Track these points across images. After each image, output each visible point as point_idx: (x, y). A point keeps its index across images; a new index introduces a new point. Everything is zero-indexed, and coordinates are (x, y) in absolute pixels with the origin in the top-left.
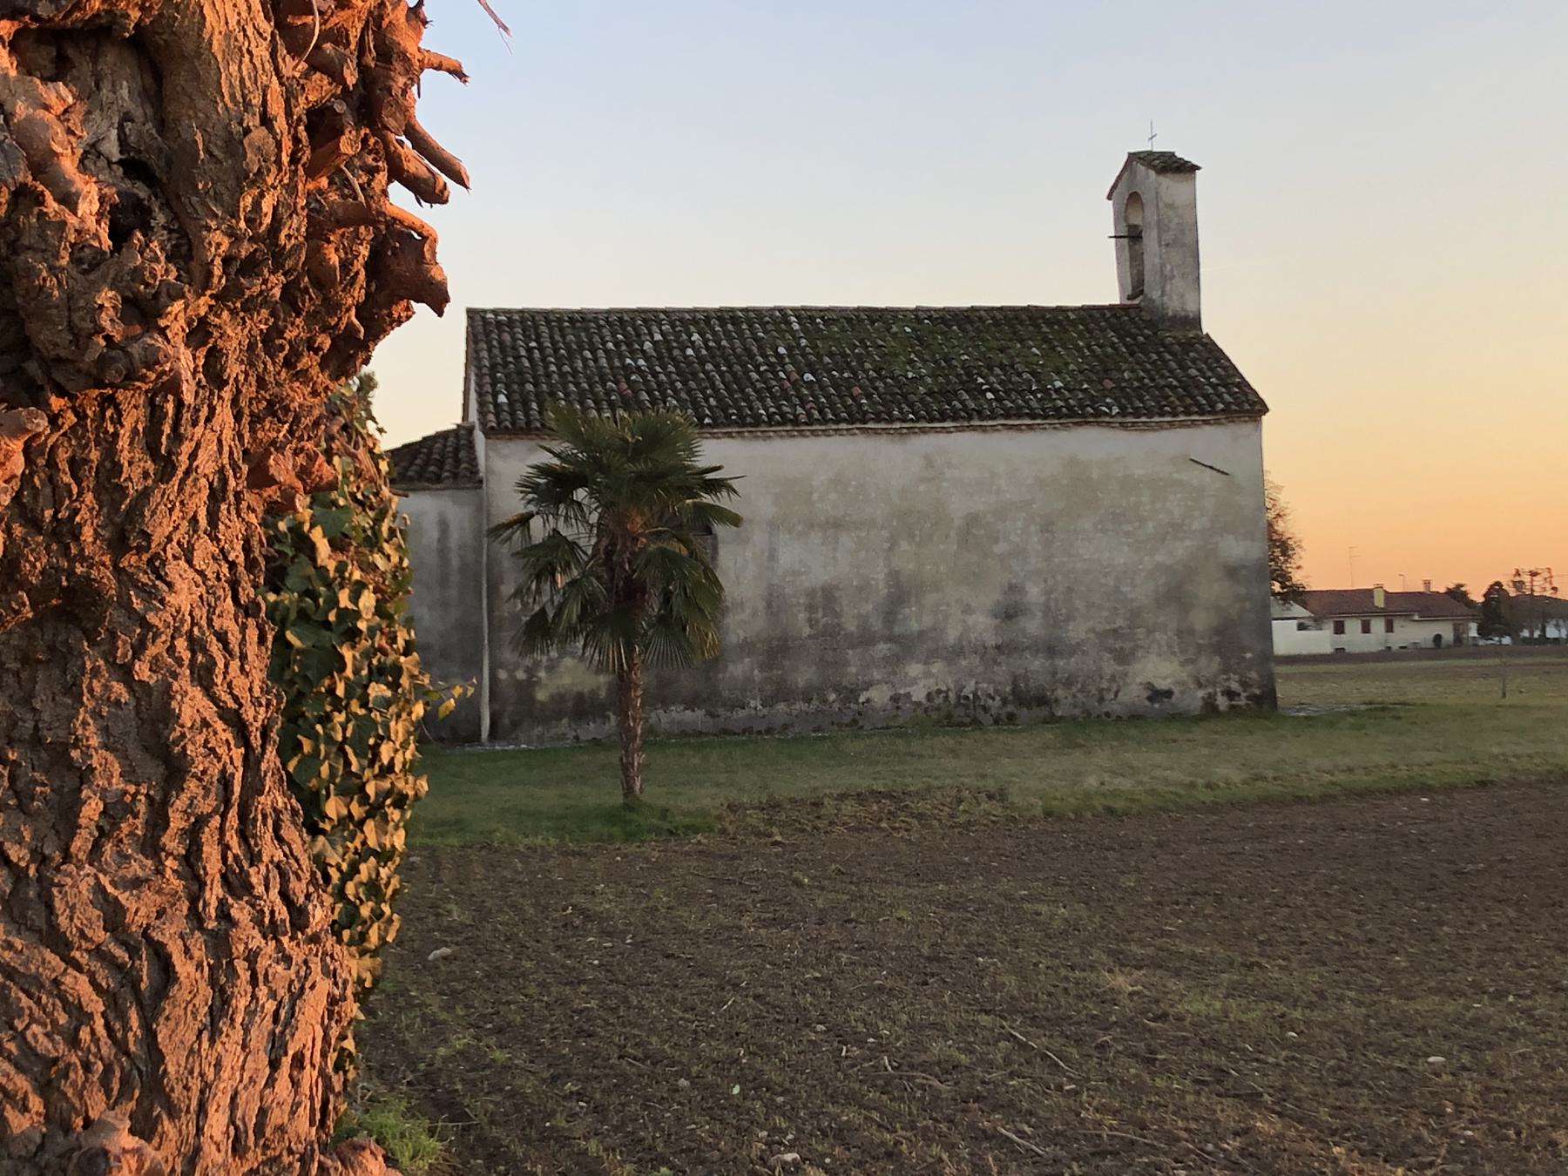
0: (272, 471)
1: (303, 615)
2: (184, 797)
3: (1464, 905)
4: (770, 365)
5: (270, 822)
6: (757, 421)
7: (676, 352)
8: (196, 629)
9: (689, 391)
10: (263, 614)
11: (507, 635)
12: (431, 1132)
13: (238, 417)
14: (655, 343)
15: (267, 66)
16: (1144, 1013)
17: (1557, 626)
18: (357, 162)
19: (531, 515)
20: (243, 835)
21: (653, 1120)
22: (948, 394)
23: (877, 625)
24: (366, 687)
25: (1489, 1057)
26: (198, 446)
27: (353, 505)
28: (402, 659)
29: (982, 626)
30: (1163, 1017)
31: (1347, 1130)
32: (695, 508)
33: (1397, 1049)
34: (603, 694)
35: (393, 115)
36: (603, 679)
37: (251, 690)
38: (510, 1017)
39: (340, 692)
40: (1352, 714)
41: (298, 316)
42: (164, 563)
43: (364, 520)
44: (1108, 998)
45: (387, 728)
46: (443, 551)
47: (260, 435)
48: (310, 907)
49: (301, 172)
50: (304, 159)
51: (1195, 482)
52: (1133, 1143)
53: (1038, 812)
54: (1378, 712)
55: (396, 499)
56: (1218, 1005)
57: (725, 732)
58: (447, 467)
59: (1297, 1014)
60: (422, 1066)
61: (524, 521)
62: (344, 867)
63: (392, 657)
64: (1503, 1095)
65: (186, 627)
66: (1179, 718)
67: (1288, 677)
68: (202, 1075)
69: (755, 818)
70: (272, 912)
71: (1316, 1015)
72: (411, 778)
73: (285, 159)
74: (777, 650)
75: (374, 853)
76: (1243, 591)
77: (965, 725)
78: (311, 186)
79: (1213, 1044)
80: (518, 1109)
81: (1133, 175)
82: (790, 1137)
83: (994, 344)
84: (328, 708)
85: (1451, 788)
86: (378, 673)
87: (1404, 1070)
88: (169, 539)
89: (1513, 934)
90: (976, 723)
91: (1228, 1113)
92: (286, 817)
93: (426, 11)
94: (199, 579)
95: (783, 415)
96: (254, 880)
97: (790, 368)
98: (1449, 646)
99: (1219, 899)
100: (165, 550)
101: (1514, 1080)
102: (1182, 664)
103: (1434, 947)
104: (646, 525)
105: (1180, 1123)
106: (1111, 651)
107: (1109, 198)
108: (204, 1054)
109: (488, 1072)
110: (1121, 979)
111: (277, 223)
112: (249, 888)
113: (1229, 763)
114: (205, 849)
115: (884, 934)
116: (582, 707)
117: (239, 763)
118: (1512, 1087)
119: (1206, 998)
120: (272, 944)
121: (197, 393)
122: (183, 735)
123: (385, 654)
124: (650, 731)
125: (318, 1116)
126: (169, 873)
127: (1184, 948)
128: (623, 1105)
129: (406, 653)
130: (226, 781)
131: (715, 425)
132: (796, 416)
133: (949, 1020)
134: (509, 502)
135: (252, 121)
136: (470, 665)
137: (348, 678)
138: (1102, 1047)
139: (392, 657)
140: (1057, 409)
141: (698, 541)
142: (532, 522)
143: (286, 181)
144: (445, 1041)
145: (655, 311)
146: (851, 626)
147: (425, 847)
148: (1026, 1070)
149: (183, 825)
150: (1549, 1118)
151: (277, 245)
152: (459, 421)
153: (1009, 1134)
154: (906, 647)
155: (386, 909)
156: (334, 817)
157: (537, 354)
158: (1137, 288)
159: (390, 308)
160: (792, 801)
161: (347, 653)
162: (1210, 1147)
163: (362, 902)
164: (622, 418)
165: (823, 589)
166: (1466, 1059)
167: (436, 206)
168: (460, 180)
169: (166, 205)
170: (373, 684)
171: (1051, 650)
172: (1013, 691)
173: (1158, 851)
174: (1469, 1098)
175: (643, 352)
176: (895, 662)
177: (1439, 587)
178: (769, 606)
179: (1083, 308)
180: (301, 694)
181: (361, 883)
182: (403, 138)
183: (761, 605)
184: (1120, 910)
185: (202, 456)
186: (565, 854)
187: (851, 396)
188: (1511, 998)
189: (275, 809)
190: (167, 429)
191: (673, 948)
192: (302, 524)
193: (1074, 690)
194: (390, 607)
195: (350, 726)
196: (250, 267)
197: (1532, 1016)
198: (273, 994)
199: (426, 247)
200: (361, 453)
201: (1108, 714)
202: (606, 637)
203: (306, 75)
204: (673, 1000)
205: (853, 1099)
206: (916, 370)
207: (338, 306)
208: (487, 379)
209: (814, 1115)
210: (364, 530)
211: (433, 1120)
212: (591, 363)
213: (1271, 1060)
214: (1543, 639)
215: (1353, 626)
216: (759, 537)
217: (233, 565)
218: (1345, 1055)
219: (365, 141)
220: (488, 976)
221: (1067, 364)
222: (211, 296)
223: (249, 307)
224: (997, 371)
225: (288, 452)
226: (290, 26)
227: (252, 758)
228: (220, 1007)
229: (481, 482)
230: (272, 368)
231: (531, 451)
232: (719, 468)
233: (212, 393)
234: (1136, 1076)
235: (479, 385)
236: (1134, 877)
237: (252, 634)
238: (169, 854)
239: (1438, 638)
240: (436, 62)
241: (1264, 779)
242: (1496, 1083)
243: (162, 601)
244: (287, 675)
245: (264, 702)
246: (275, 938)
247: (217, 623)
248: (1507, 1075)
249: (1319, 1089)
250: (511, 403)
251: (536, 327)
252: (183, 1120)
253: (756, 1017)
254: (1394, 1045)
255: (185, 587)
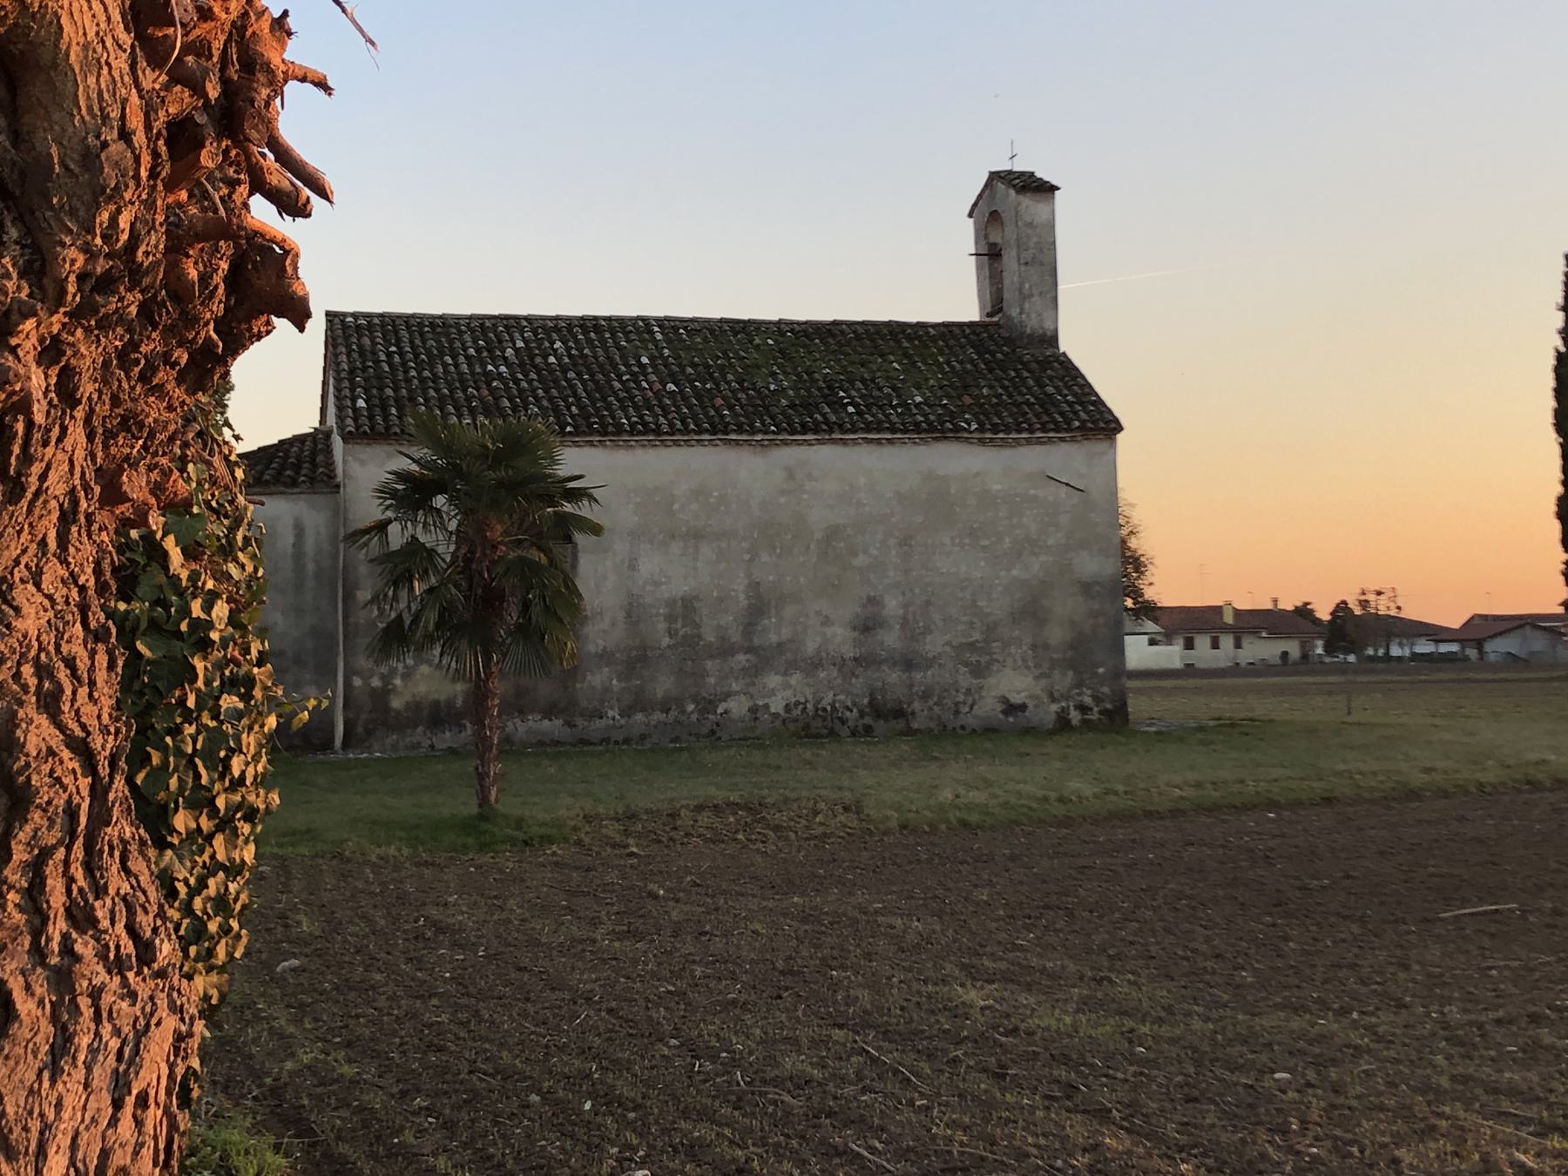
0: (124, 487)
1: (154, 625)
2: (28, 828)
3: (1309, 921)
4: (633, 374)
5: (117, 853)
6: (619, 430)
7: (538, 360)
8: (43, 656)
9: (551, 399)
10: (113, 640)
11: (363, 642)
12: (277, 1148)
13: (90, 437)
14: (517, 350)
15: (126, 78)
16: (995, 1027)
17: (1401, 645)
18: (218, 175)
19: (389, 521)
20: (89, 868)
21: (503, 1136)
22: (809, 406)
23: (736, 636)
24: (218, 698)
25: (1333, 1074)
26: (48, 467)
27: (207, 513)
28: (256, 670)
29: (841, 639)
30: (1014, 1031)
31: (1195, 1146)
32: (555, 517)
33: (1243, 1066)
34: (459, 702)
35: (255, 127)
36: (460, 687)
37: (99, 717)
38: (359, 1030)
39: (191, 703)
40: (1201, 729)
41: (154, 330)
42: (11, 587)
43: (218, 529)
44: (959, 1012)
45: (238, 740)
46: (299, 567)
47: (113, 450)
48: (157, 941)
49: (160, 187)
50: (164, 174)
51: (1051, 498)
52: (983, 1159)
53: (893, 824)
54: (1229, 729)
55: (251, 507)
56: (1068, 1020)
57: (583, 742)
58: (304, 472)
59: (1145, 1029)
60: (268, 1080)
61: (382, 527)
62: (192, 881)
63: (245, 668)
64: (1346, 1112)
65: (33, 653)
66: (1029, 731)
67: (1139, 691)
68: (42, 1115)
69: (612, 830)
70: (118, 947)
71: (1164, 1031)
72: (262, 792)
73: (144, 174)
74: (637, 660)
75: (223, 867)
76: (1097, 606)
77: (822, 736)
78: (170, 200)
79: (1065, 1060)
80: (366, 1125)
81: (992, 197)
82: (641, 1153)
83: (856, 358)
84: (179, 720)
85: (1297, 804)
86: (230, 685)
87: (1252, 1087)
88: (17, 562)
89: (1356, 950)
90: (832, 733)
91: (1077, 1129)
92: (133, 847)
93: (291, 22)
94: (46, 603)
95: (645, 424)
96: (99, 914)
97: (653, 378)
98: (1295, 664)
99: (1070, 913)
100: (12, 574)
101: (1358, 1097)
102: (1037, 678)
103: (1279, 963)
104: (506, 533)
105: (1030, 1140)
106: (967, 665)
107: (970, 215)
108: (44, 1094)
109: (335, 1087)
110: (973, 994)
111: (134, 240)
112: (94, 922)
113: (1083, 778)
114: (49, 881)
115: (738, 947)
116: (438, 716)
117: (85, 792)
118: (1355, 1103)
119: (1057, 1011)
120: (117, 980)
121: (48, 413)
122: (28, 765)
123: (238, 665)
124: (507, 739)
125: (162, 1157)
126: (10, 907)
127: (1034, 962)
128: (472, 1121)
129: (259, 665)
130: (72, 813)
131: (576, 433)
132: (659, 426)
133: (804, 1034)
134: (367, 508)
135: (110, 135)
136: (325, 673)
137: (199, 690)
138: (955, 1061)
139: (245, 668)
140: (917, 424)
141: (557, 549)
142: (390, 527)
143: (144, 196)
144: (293, 1055)
145: (516, 318)
146: (710, 637)
147: (275, 856)
148: (879, 1086)
149: (26, 857)
150: (1392, 1136)
151: (134, 262)
152: (317, 425)
153: (861, 1150)
154: (763, 659)
155: (235, 924)
156: (183, 830)
157: (397, 358)
158: (995, 301)
159: (250, 323)
160: (648, 812)
161: (199, 665)
162: (1059, 1163)
163: (209, 918)
164: (483, 425)
165: (682, 599)
166: (1311, 1075)
167: (299, 220)
168: (323, 193)
169: (19, 219)
170: (225, 696)
171: (908, 664)
172: (870, 703)
173: (1010, 865)
174: (1314, 1115)
175: (505, 358)
176: (753, 673)
177: (1287, 604)
178: (629, 615)
179: (944, 325)
180: (150, 707)
181: (209, 898)
182: (266, 151)
183: (621, 615)
184: (973, 924)
185: (53, 477)
186: (417, 864)
187: (713, 406)
188: (1355, 1015)
189: (122, 840)
190: (16, 450)
191: (525, 962)
192: (155, 532)
193: (931, 703)
194: (244, 617)
195: (200, 738)
196: (106, 284)
197: (1376, 1033)
198: (117, 1032)
199: (288, 262)
200: (217, 460)
201: (963, 727)
202: (464, 644)
203: (167, 87)
204: (524, 1014)
205: (706, 1115)
206: (779, 384)
207: (197, 319)
208: (346, 383)
209: (664, 1131)
210: (219, 539)
211: (280, 1136)
212: (452, 369)
213: (1120, 1075)
214: (1388, 658)
215: (1203, 642)
216: (620, 547)
217: (82, 589)
218: (1192, 1070)
219: (226, 152)
220: (337, 988)
221: (927, 380)
222: (65, 314)
223: (104, 325)
224: (859, 385)
225: (142, 469)
226: (151, 38)
227: (99, 787)
228: (62, 1046)
229: (338, 486)
230: (125, 383)
231: (389, 456)
232: (581, 477)
233: (64, 413)
234: (986, 1091)
235: (338, 389)
236: (986, 891)
237: (102, 659)
238: (11, 887)
239: (1285, 654)
240: (300, 74)
241: (1116, 793)
242: (1341, 1100)
243: (8, 626)
244: (136, 686)
245: (112, 730)
246: (120, 973)
247: (65, 649)
248: (1352, 1092)
249: (1168, 1106)
250: (369, 408)
251: (396, 332)
252: (21, 1161)
253: (611, 1031)
254: (1241, 1061)
255: (33, 611)
